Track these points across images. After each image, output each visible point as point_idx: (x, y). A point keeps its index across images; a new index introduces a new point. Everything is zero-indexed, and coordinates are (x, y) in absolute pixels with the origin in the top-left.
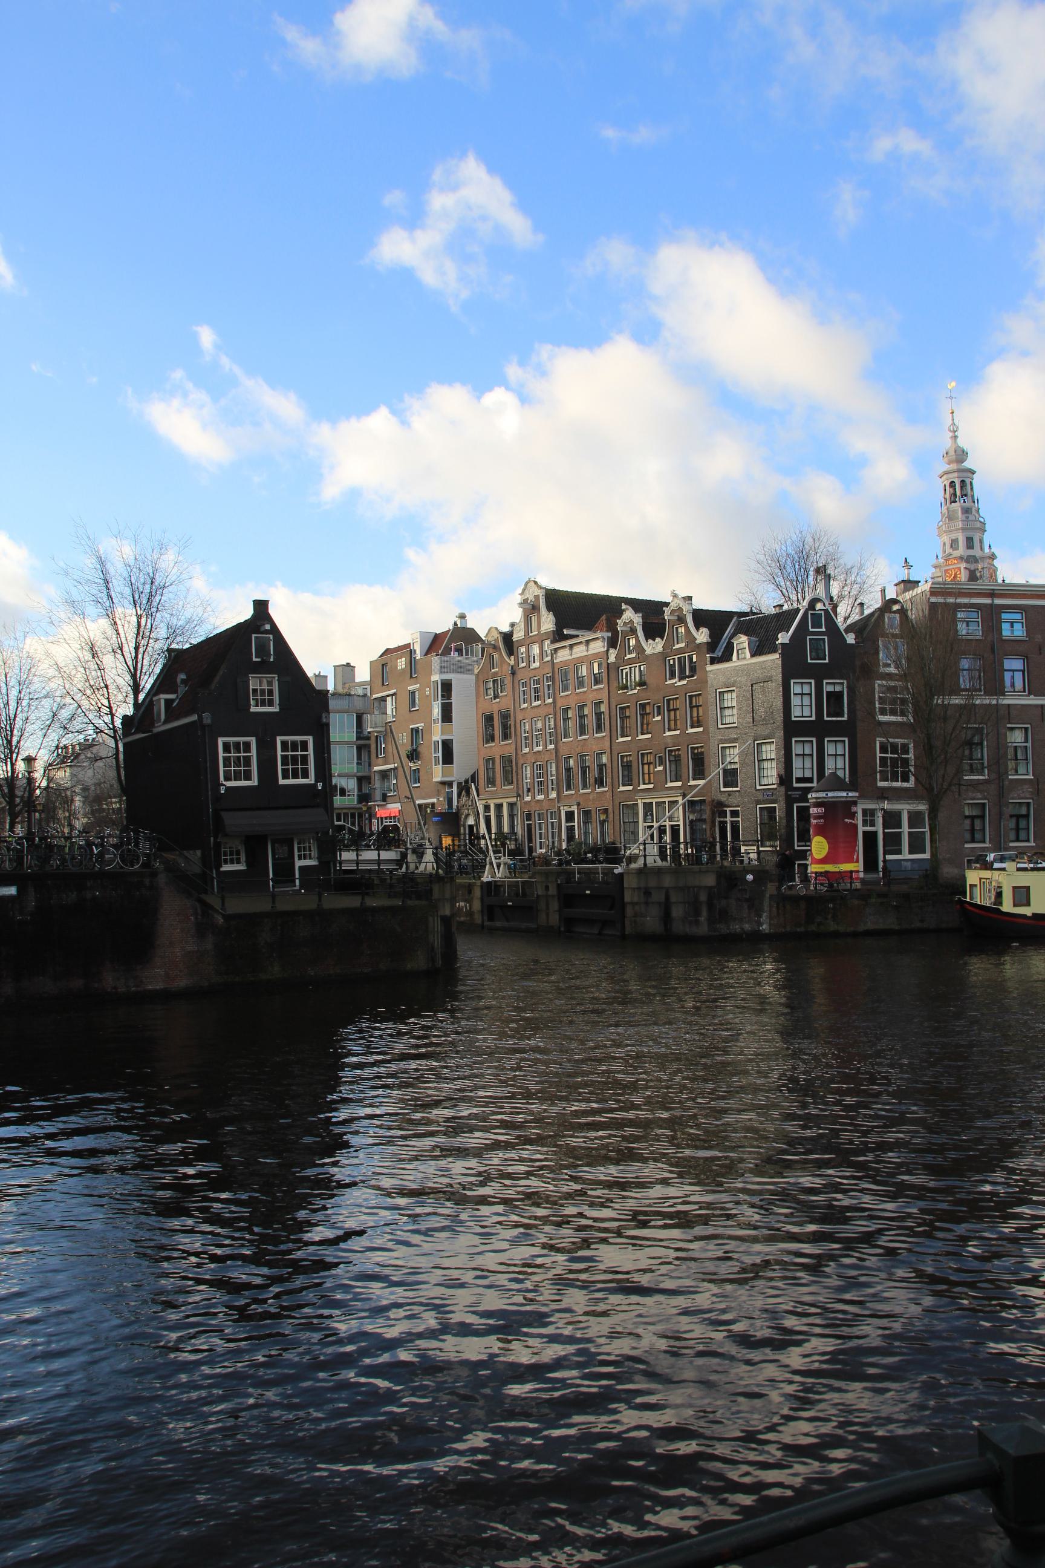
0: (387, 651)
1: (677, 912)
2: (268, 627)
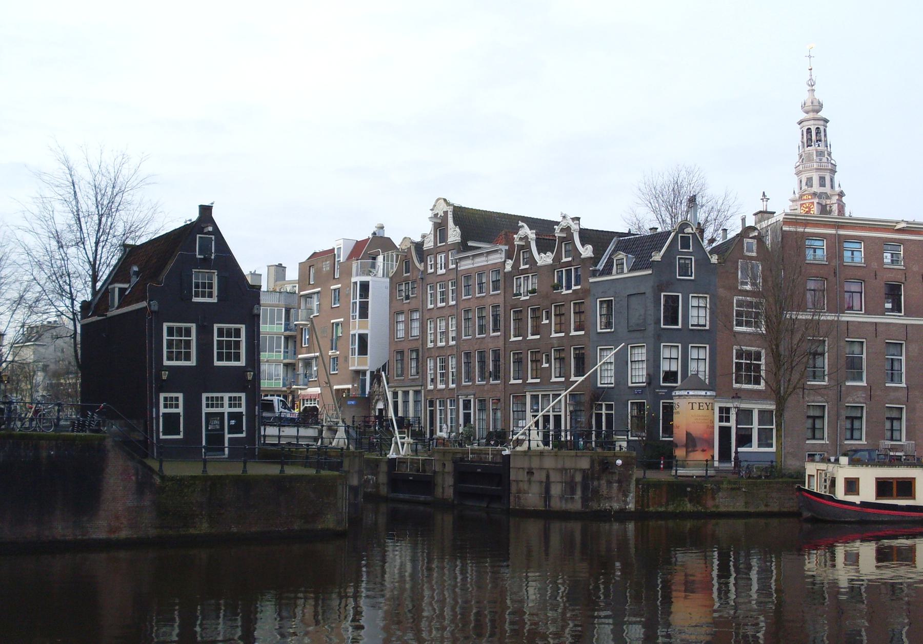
0: (315, 255)
1: (556, 490)
2: (210, 229)
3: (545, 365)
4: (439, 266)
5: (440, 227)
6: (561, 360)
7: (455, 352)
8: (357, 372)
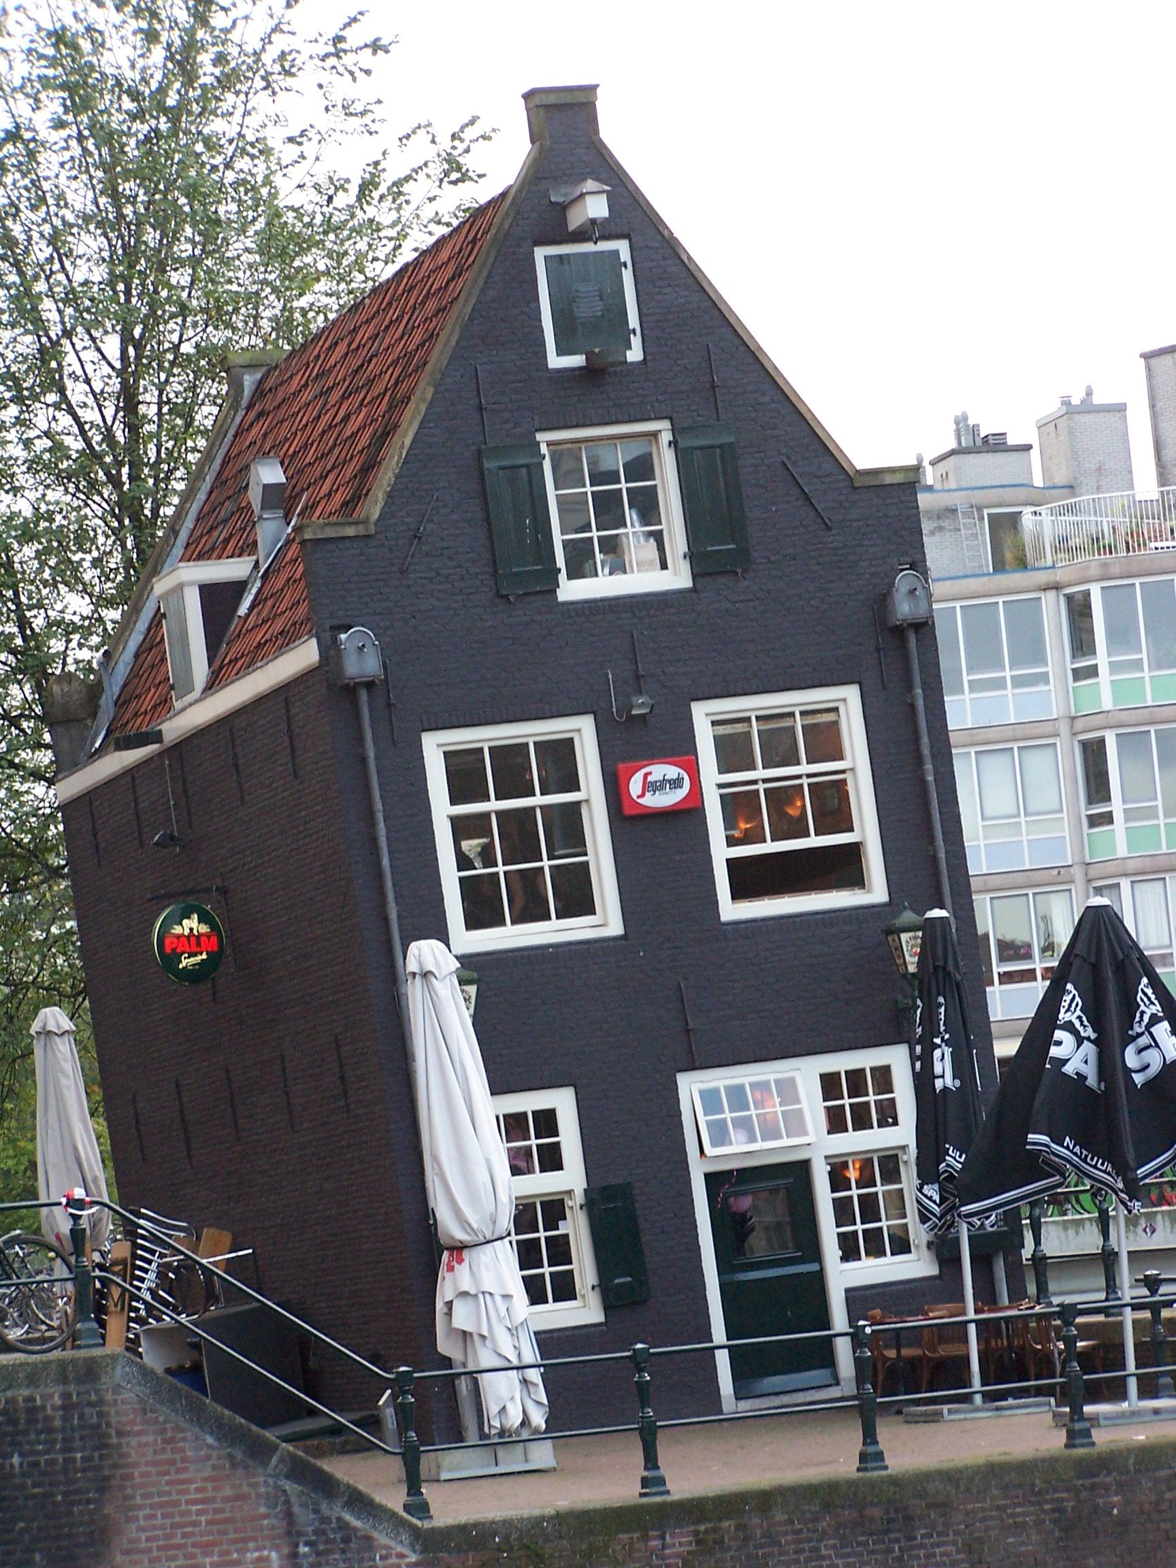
2: (597, 207)
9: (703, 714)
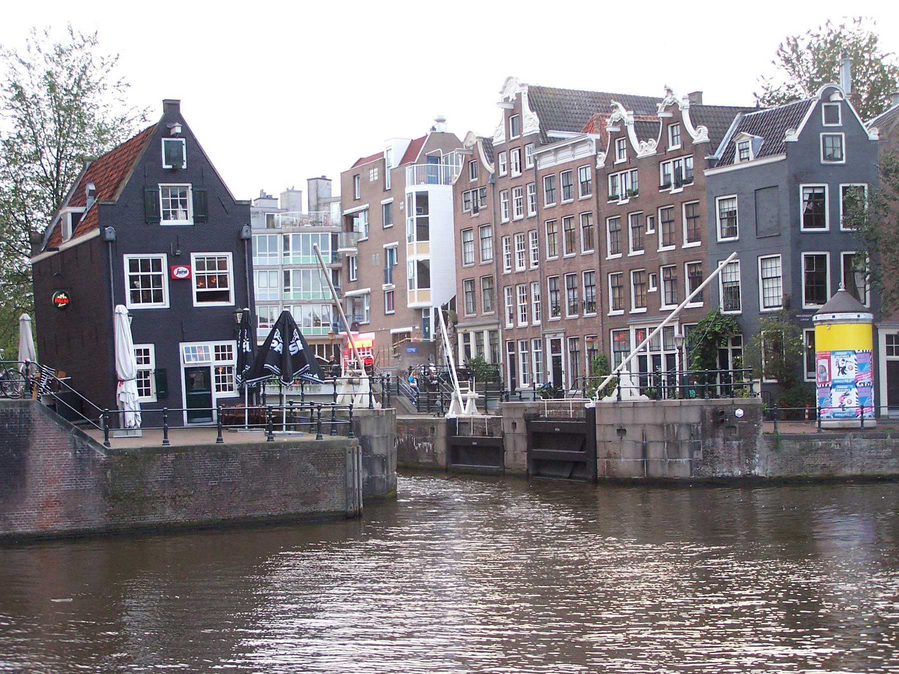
0: (360, 161)
1: (655, 452)
2: (178, 130)
3: (653, 289)
4: (509, 167)
5: (513, 116)
6: (673, 281)
7: (538, 278)
8: (418, 310)
9: (193, 256)
